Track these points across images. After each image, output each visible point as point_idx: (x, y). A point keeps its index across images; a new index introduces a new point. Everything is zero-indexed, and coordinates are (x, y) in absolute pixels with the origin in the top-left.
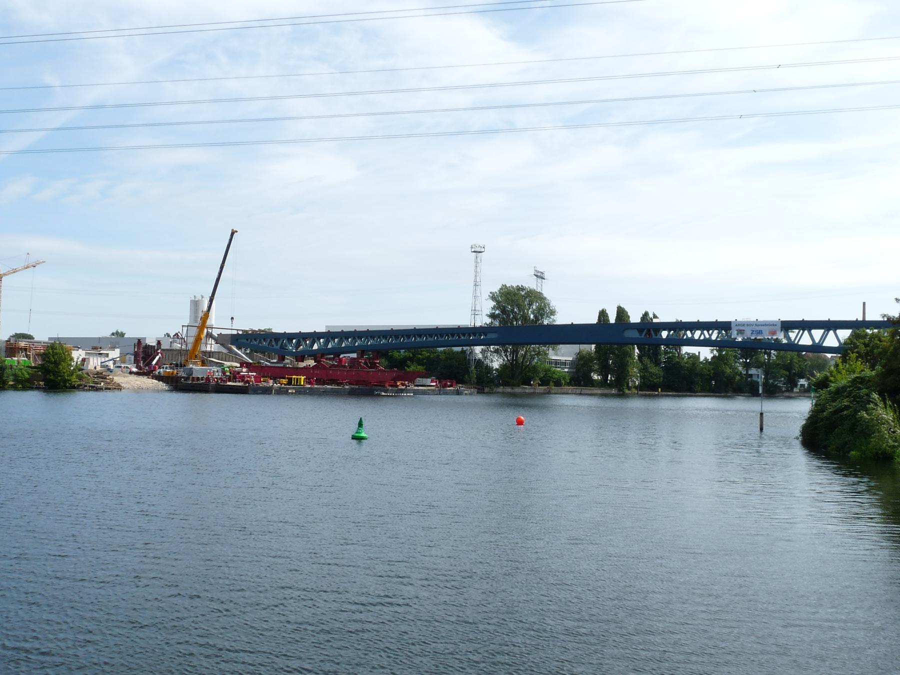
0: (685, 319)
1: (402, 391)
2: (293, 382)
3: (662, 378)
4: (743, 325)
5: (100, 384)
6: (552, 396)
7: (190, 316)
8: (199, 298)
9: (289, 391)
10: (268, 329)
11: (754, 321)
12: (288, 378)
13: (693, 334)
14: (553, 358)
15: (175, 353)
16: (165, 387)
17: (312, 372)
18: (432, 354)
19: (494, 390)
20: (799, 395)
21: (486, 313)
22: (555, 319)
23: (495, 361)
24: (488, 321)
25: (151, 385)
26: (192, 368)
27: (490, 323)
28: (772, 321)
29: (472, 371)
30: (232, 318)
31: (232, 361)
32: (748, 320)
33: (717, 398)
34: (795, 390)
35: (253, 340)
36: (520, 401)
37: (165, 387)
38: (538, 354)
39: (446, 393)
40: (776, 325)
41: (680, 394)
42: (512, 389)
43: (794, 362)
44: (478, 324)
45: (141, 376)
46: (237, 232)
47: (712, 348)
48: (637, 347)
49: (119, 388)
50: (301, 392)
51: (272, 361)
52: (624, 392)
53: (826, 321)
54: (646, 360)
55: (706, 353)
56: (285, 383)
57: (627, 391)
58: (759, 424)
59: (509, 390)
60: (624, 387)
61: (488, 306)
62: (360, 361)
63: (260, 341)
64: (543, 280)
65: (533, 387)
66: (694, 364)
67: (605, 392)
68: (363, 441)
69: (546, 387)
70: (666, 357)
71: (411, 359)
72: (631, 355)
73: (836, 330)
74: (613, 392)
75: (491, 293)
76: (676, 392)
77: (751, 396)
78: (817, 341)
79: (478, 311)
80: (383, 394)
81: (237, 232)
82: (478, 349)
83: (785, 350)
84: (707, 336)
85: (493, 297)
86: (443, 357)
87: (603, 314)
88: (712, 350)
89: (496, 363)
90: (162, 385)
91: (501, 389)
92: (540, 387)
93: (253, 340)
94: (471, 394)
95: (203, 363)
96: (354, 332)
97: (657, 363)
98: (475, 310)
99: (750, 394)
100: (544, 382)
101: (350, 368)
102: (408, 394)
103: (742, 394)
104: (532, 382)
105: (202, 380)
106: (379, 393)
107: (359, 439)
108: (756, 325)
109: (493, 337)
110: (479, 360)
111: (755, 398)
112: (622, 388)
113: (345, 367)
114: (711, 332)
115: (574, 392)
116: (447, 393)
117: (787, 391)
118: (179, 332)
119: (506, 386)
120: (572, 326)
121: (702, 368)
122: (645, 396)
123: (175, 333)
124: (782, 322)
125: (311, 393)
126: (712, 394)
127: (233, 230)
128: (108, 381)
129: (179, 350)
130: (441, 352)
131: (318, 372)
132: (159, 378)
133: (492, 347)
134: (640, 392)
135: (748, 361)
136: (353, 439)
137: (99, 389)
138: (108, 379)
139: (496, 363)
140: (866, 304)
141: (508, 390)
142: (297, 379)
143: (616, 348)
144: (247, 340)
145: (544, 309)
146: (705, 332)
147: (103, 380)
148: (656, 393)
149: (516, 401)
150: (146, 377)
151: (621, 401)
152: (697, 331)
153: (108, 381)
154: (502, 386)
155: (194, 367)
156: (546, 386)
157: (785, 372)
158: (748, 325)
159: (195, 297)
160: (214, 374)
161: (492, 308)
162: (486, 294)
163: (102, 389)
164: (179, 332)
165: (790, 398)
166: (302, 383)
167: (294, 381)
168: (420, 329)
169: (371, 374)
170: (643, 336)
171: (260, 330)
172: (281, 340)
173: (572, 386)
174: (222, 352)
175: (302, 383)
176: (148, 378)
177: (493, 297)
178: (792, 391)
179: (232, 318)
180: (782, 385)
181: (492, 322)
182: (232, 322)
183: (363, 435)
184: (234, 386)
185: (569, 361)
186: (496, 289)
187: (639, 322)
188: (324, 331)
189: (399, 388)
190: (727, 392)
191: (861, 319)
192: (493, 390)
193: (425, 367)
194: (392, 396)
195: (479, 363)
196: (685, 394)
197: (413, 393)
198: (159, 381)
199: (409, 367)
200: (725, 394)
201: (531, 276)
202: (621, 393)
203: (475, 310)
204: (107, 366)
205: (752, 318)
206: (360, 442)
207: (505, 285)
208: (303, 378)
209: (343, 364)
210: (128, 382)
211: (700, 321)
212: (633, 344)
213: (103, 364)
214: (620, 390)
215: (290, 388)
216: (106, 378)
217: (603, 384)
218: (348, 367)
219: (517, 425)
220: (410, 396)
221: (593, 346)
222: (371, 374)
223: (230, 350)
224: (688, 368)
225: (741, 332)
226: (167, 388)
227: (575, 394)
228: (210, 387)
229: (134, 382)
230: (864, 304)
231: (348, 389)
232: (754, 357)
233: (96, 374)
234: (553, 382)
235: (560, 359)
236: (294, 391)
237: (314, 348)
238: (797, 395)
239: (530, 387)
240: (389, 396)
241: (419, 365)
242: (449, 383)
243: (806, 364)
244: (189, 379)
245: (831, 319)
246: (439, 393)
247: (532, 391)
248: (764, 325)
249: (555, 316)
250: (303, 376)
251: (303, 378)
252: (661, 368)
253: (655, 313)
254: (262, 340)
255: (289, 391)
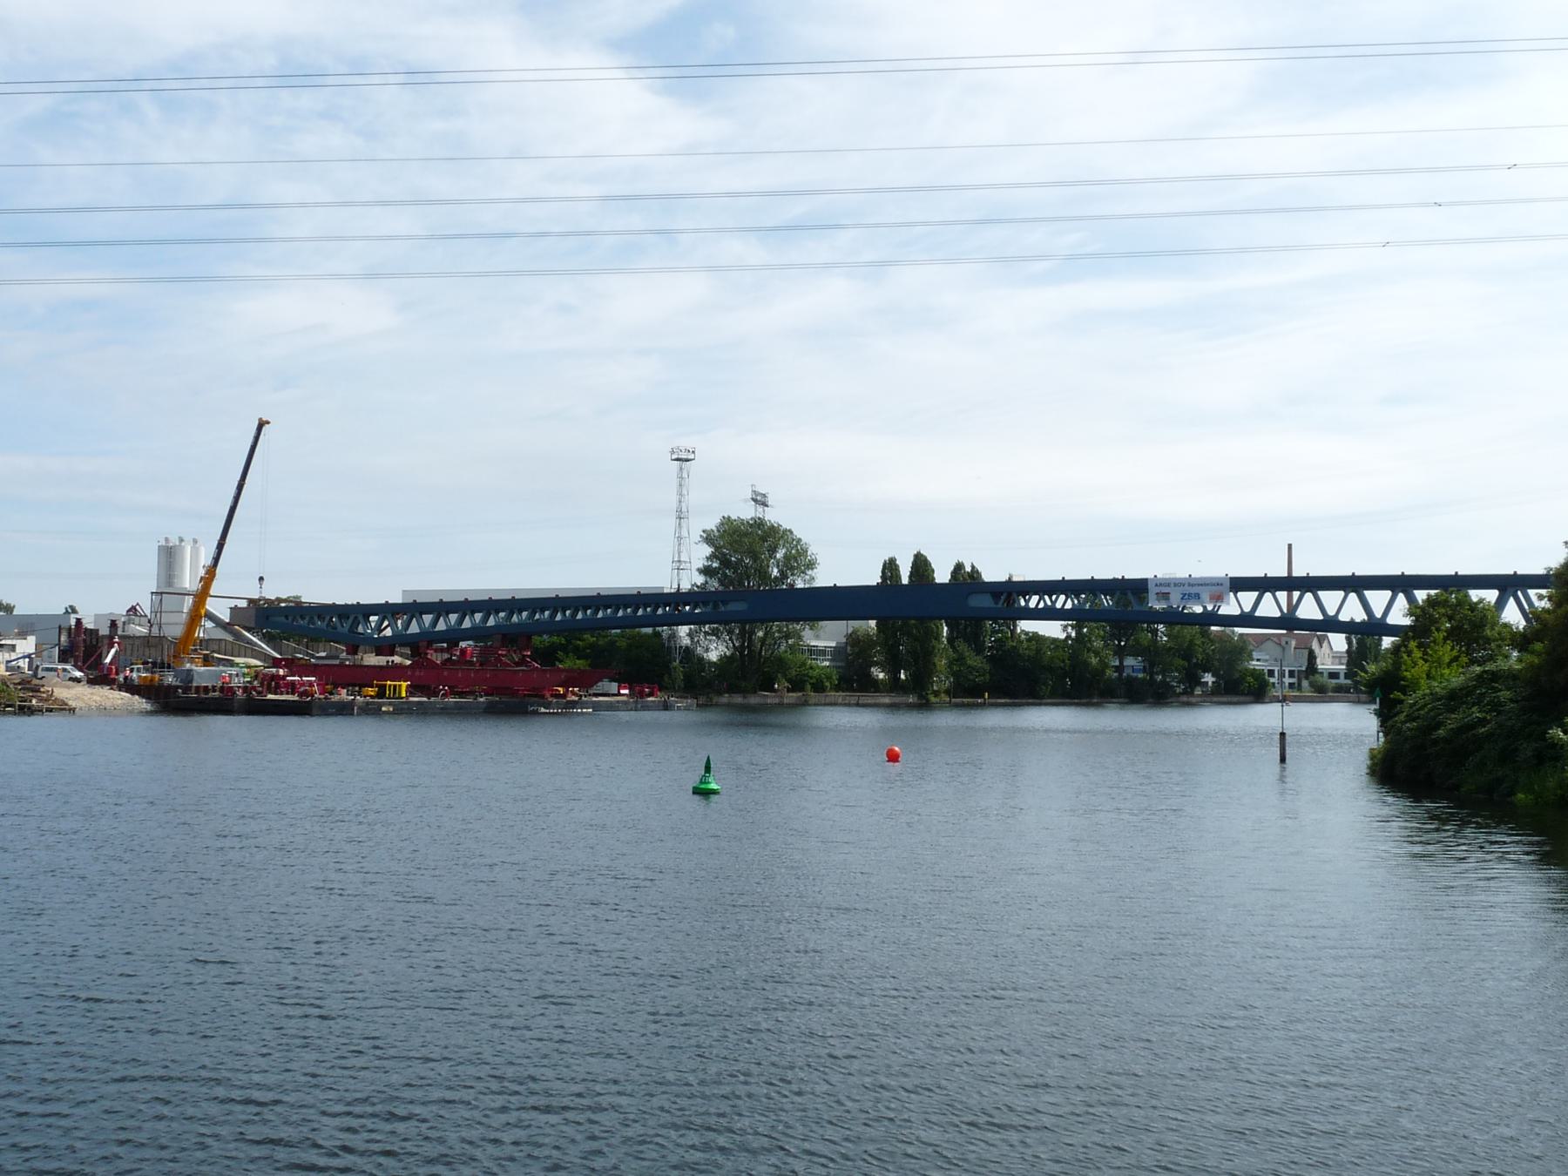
0: (1524, 570)
1: (573, 704)
2: (388, 692)
3: (988, 676)
4: (1169, 585)
5: (31, 701)
6: (809, 708)
7: (158, 575)
8: (174, 541)
9: (384, 709)
10: (294, 597)
11: (1186, 578)
12: (377, 686)
13: (1027, 602)
14: (812, 644)
15: (137, 642)
16: (145, 706)
17: (409, 673)
18: (601, 639)
19: (714, 701)
20: (1202, 699)
21: (697, 567)
22: (813, 575)
23: (712, 650)
24: (700, 580)
25: (120, 702)
26: (191, 670)
27: (702, 584)
28: (1215, 578)
29: (675, 668)
30: (261, 579)
31: (245, 656)
32: (1172, 576)
33: (1078, 708)
34: (1198, 691)
35: (298, 617)
36: (752, 717)
37: (145, 706)
38: (787, 636)
39: (646, 708)
40: (1222, 585)
41: (1016, 701)
42: (745, 697)
43: (1196, 644)
44: (686, 586)
45: (97, 687)
46: (268, 423)
47: (1066, 623)
48: (946, 623)
49: (64, 708)
50: (402, 710)
51: (317, 655)
52: (928, 700)
53: (1451, 576)
54: (962, 646)
55: (1053, 629)
56: (372, 694)
57: (933, 699)
58: (1279, 753)
59: (738, 699)
60: (929, 692)
61: (700, 554)
62: (500, 652)
63: (312, 618)
64: (766, 508)
65: (779, 693)
66: (1038, 651)
67: (897, 701)
68: (711, 796)
69: (800, 694)
70: (993, 639)
71: (564, 648)
72: (938, 636)
73: (1237, 592)
74: (911, 700)
75: (704, 531)
76: (1011, 699)
77: (1126, 703)
78: (1378, 614)
79: (685, 562)
80: (543, 710)
81: (268, 423)
82: (683, 630)
83: (1182, 624)
84: (1049, 603)
85: (709, 539)
86: (623, 643)
87: (890, 567)
88: (1065, 627)
89: (715, 651)
90: (139, 703)
91: (725, 699)
92: (791, 694)
93: (298, 617)
94: (687, 709)
95: (207, 661)
96: (439, 603)
97: (979, 650)
98: (679, 561)
99: (1126, 700)
100: (797, 685)
101: (481, 665)
102: (584, 710)
103: (1114, 700)
104: (776, 686)
105: (214, 691)
106: (536, 708)
107: (703, 793)
108: (1189, 585)
109: (740, 609)
110: (687, 647)
111: (1135, 706)
112: (924, 693)
113: (471, 663)
114: (1054, 597)
115: (847, 702)
116: (647, 706)
117: (1185, 693)
118: (138, 604)
119: (733, 693)
120: (835, 590)
121: (1052, 658)
122: (957, 706)
123: (130, 606)
124: (1231, 578)
125: (422, 712)
126: (1067, 701)
127: (260, 419)
128: (45, 695)
129: (146, 637)
130: (617, 635)
131: (422, 674)
132: (129, 687)
133: (707, 626)
134: (953, 700)
135: (1123, 643)
136: (694, 793)
137: (36, 711)
138: (44, 692)
139: (714, 653)
140: (1293, 547)
141: (738, 699)
142: (395, 686)
143: (914, 624)
144: (287, 617)
145: (799, 560)
146: (1046, 597)
147: (35, 694)
148: (979, 701)
149: (752, 718)
150: (108, 687)
151: (921, 715)
152: (1034, 597)
153: (45, 695)
154: (728, 692)
155: (194, 668)
156: (800, 691)
157: (1182, 662)
158: (1175, 585)
159: (167, 540)
160: (230, 681)
161: (707, 558)
162: (696, 534)
163: (41, 711)
164: (138, 604)
165: (1189, 704)
166: (404, 694)
167: (390, 690)
168: (608, 596)
169: (521, 674)
170: (1000, 605)
171: (279, 600)
172: (328, 618)
173: (843, 692)
174: (225, 640)
175: (404, 694)
176: (112, 689)
177: (709, 539)
178: (1191, 694)
179: (261, 579)
180: (1175, 684)
181: (706, 582)
182: (261, 584)
183: (713, 786)
184: (283, 701)
185: (831, 647)
186: (712, 523)
187: (948, 581)
188: (400, 601)
189: (568, 699)
190: (1090, 696)
191: (1286, 575)
192: (711, 699)
193: (589, 662)
194: (557, 713)
195: (688, 652)
196: (1024, 701)
197: (593, 708)
198: (133, 694)
199: (561, 661)
200: (1088, 700)
201: (746, 501)
202: (924, 701)
203: (679, 561)
204: (19, 667)
205: (1182, 573)
206: (707, 799)
207: (729, 517)
208: (404, 685)
209: (468, 659)
210: (79, 698)
211: (1268, 575)
212: (941, 619)
213: (9, 665)
214: (921, 697)
215: (384, 704)
216: (39, 691)
217: (894, 686)
218: (478, 665)
219: (888, 761)
220: (586, 713)
221: (873, 623)
222: (521, 674)
223: (238, 636)
224: (1029, 656)
225: (1165, 596)
226: (148, 707)
227: (849, 705)
228: (236, 704)
229: (89, 696)
230: (1290, 546)
231: (483, 702)
232: (1132, 638)
233: (19, 684)
234: (810, 684)
235: (816, 644)
236: (391, 709)
237: (463, 627)
238: (1199, 699)
239: (773, 694)
240: (553, 713)
241: (578, 659)
242: (647, 690)
243: (1213, 647)
244: (191, 690)
245: (1126, 577)
246: (636, 707)
247: (777, 701)
248: (1202, 585)
249: (815, 570)
250: (405, 681)
251: (404, 685)
252: (985, 657)
253: (975, 564)
254: (316, 618)
255: (384, 709)
